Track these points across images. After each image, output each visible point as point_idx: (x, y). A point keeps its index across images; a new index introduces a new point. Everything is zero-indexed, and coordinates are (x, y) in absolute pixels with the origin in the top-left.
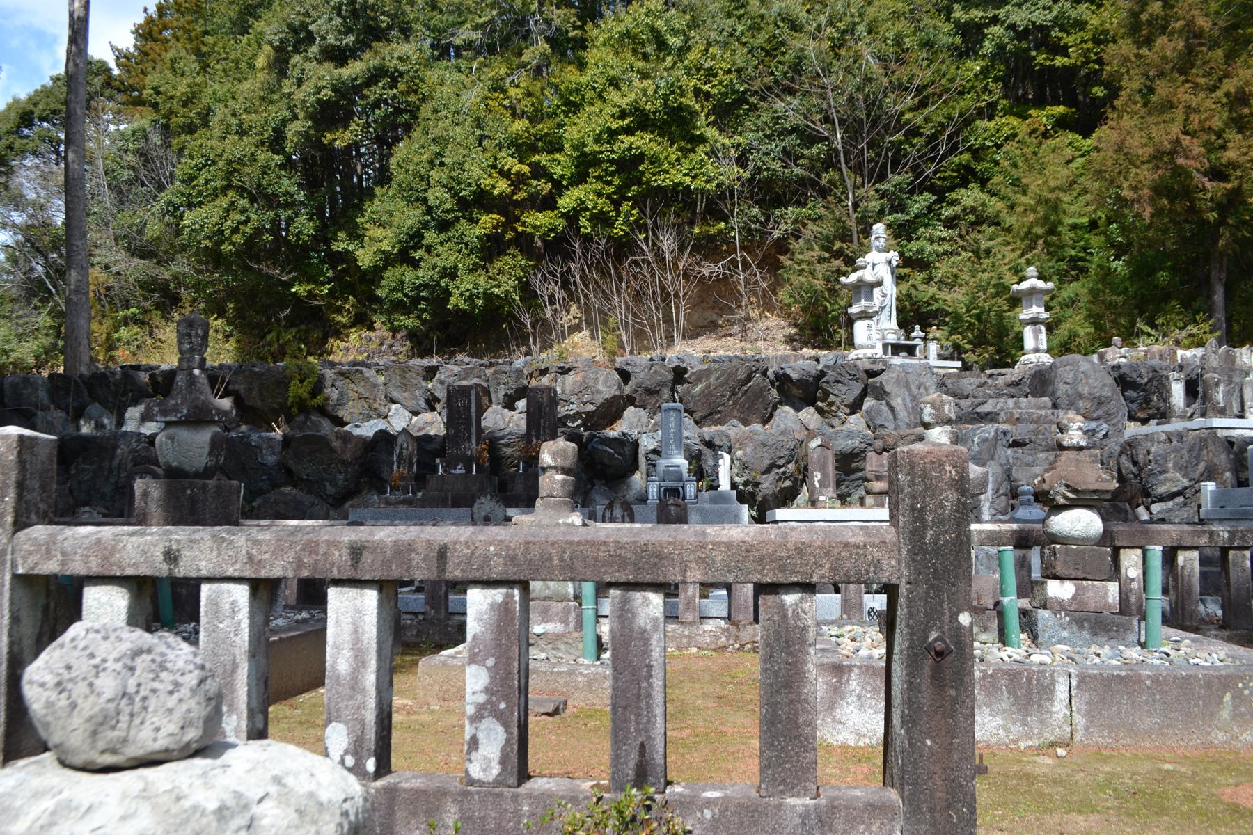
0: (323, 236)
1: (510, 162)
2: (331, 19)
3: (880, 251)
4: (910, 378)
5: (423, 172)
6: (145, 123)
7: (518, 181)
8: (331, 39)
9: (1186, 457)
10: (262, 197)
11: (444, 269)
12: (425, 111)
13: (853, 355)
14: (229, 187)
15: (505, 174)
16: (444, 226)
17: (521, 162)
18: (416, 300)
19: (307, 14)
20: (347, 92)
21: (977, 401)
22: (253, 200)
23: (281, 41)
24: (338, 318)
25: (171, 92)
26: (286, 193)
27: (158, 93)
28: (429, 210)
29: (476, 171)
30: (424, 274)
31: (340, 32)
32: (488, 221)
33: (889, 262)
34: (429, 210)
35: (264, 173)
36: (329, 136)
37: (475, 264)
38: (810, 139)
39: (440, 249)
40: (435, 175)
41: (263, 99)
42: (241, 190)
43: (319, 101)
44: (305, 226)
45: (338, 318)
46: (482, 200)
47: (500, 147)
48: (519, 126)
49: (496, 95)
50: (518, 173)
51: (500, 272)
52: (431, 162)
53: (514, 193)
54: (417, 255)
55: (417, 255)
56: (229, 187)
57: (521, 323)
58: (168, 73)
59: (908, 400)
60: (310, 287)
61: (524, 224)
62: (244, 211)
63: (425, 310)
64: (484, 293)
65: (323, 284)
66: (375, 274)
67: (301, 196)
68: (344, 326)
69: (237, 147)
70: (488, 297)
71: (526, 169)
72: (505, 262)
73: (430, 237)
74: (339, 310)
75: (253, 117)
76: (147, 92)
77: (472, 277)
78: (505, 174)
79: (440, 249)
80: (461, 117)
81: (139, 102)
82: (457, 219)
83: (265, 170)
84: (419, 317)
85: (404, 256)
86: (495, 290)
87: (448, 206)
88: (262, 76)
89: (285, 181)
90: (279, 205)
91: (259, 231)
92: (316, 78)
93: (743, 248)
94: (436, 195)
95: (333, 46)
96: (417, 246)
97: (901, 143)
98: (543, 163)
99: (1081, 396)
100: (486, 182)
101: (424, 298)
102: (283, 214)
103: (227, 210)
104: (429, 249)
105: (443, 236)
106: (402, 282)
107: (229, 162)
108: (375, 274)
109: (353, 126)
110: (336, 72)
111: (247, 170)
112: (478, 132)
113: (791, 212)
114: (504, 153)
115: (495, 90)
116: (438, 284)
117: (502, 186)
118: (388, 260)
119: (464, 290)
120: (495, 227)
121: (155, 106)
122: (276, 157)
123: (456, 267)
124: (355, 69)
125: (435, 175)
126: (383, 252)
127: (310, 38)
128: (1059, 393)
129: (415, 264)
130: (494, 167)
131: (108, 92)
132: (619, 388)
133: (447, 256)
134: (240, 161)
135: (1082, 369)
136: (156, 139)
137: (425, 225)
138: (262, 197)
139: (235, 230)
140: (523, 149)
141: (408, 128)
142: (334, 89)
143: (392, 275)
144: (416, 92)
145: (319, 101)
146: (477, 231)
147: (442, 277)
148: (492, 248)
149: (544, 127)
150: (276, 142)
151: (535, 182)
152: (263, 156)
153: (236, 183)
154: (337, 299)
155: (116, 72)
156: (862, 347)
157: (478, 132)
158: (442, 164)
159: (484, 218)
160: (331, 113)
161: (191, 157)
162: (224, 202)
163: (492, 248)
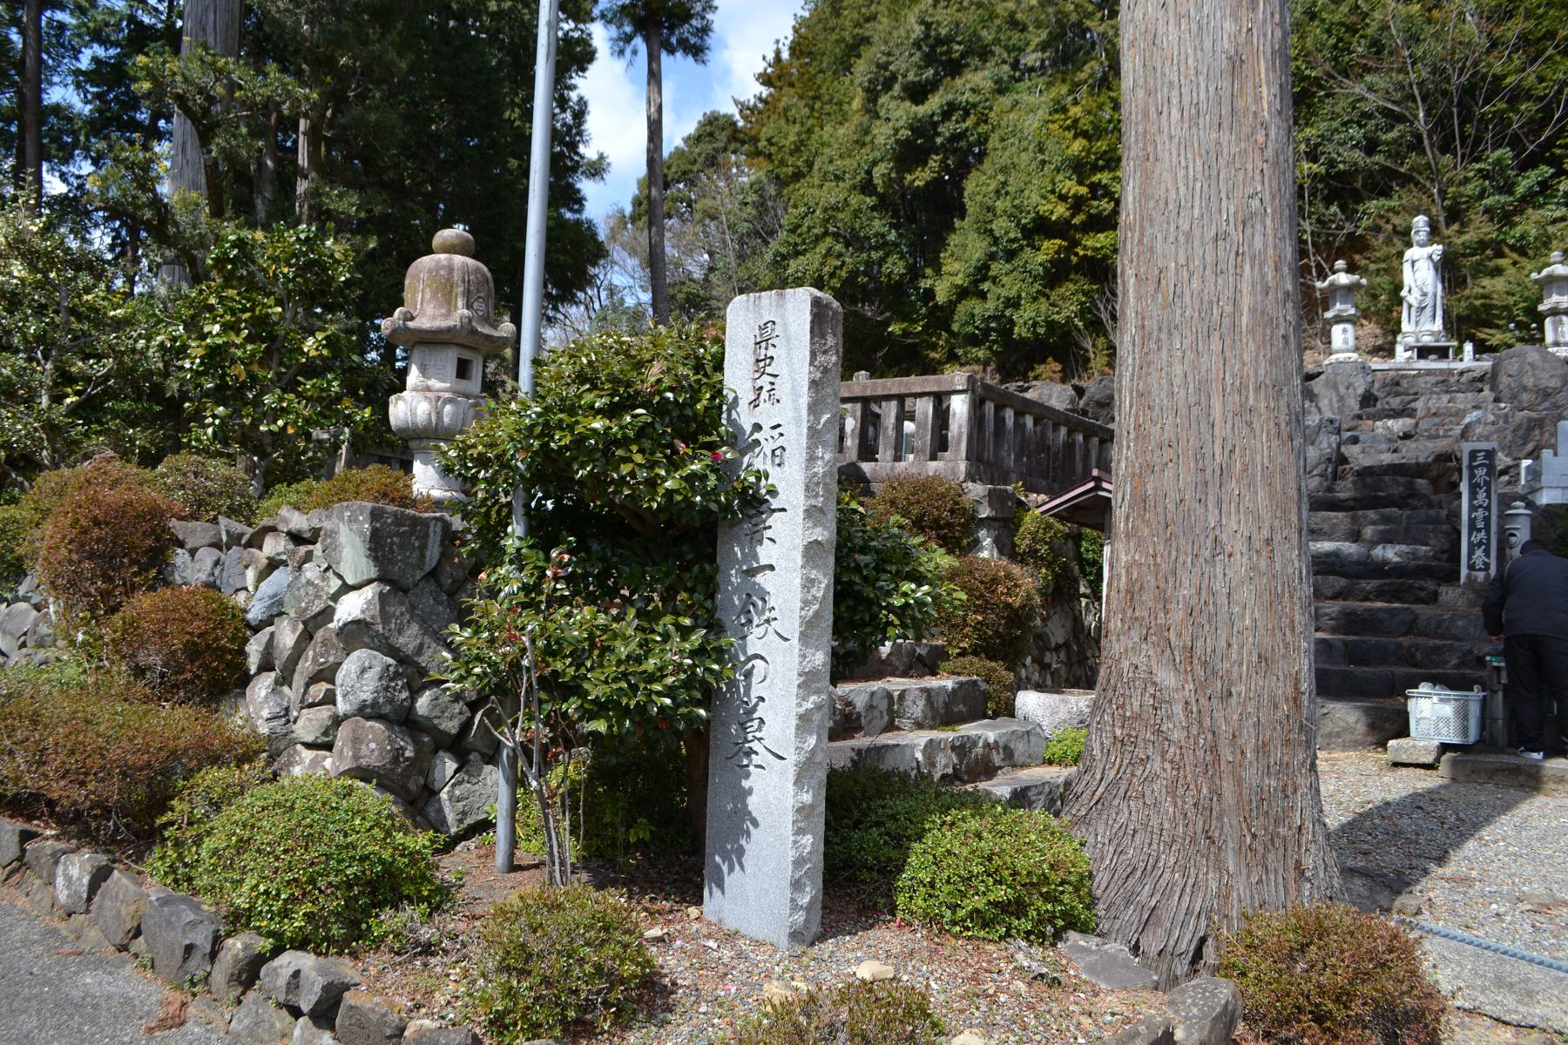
0: (915, 273)
1: (1071, 187)
2: (911, 55)
3: (1421, 246)
4: (1339, 379)
5: (990, 203)
6: (761, 174)
7: (1078, 204)
8: (911, 77)
9: (1510, 437)
10: (854, 240)
11: (1008, 299)
12: (994, 142)
13: (1333, 358)
14: (826, 234)
15: (1063, 198)
16: (1011, 255)
17: (1080, 183)
18: (987, 332)
19: (889, 54)
20: (924, 129)
21: (1408, 398)
22: (847, 245)
23: (870, 81)
24: (933, 355)
25: (783, 142)
26: (876, 235)
27: (772, 144)
28: (996, 241)
29: (1035, 198)
30: (991, 306)
31: (920, 68)
32: (1050, 246)
33: (1430, 257)
34: (996, 241)
35: (856, 217)
36: (909, 177)
37: (1038, 292)
38: (1394, 118)
39: (1005, 279)
40: (1000, 205)
41: (857, 142)
42: (836, 236)
43: (897, 141)
44: (895, 267)
45: (933, 355)
46: (1042, 227)
47: (1058, 170)
48: (1078, 146)
49: (1056, 116)
50: (1075, 196)
51: (1064, 299)
52: (997, 192)
53: (1073, 216)
54: (985, 286)
55: (985, 286)
56: (826, 234)
57: (1082, 348)
58: (783, 122)
59: (1335, 400)
60: (904, 325)
61: (1085, 248)
62: (840, 255)
63: (994, 342)
64: (1045, 321)
65: (916, 321)
66: (951, 306)
67: (892, 236)
68: (940, 363)
69: (833, 194)
70: (1051, 325)
71: (1083, 190)
72: (1068, 288)
73: (996, 268)
74: (934, 347)
75: (847, 162)
76: (762, 144)
77: (1035, 306)
78: (1063, 198)
79: (1005, 279)
80: (1025, 143)
81: (758, 153)
82: (1022, 248)
83: (856, 213)
84: (990, 348)
85: (971, 290)
86: (1056, 317)
87: (1012, 235)
88: (856, 119)
89: (877, 223)
90: (871, 248)
91: (854, 274)
92: (899, 113)
93: (1318, 252)
94: (1000, 225)
95: (913, 83)
96: (984, 279)
97: (1504, 111)
98: (1104, 181)
99: (1525, 388)
100: (1044, 208)
101: (994, 330)
102: (875, 255)
103: (825, 256)
104: (994, 280)
105: (1008, 266)
106: (973, 316)
107: (825, 210)
108: (951, 306)
109: (932, 163)
110: (914, 108)
111: (841, 216)
112: (1040, 157)
113: (1373, 205)
114: (1060, 177)
115: (1056, 111)
116: (1003, 316)
117: (1060, 211)
118: (963, 293)
119: (1025, 320)
120: (1058, 252)
121: (769, 157)
122: (868, 200)
123: (1019, 297)
124: (934, 103)
125: (1000, 205)
126: (957, 286)
127: (893, 78)
128: (1501, 387)
129: (983, 296)
130: (1053, 192)
131: (732, 146)
132: (1072, 402)
133: (1011, 285)
134: (835, 208)
135: (1529, 360)
136: (772, 190)
137: (992, 257)
138: (854, 240)
139: (832, 275)
140: (1080, 168)
141: (981, 157)
142: (911, 128)
143: (963, 308)
144: (986, 122)
145: (897, 141)
146: (1041, 258)
147: (1006, 307)
148: (1056, 274)
149: (1102, 145)
150: (867, 187)
151: (1095, 203)
152: (855, 200)
153: (832, 229)
154: (931, 336)
155: (741, 123)
156: (1337, 352)
157: (1040, 157)
158: (1007, 193)
159: (1046, 244)
160: (909, 153)
161: (795, 207)
162: (822, 249)
163: (1056, 274)
